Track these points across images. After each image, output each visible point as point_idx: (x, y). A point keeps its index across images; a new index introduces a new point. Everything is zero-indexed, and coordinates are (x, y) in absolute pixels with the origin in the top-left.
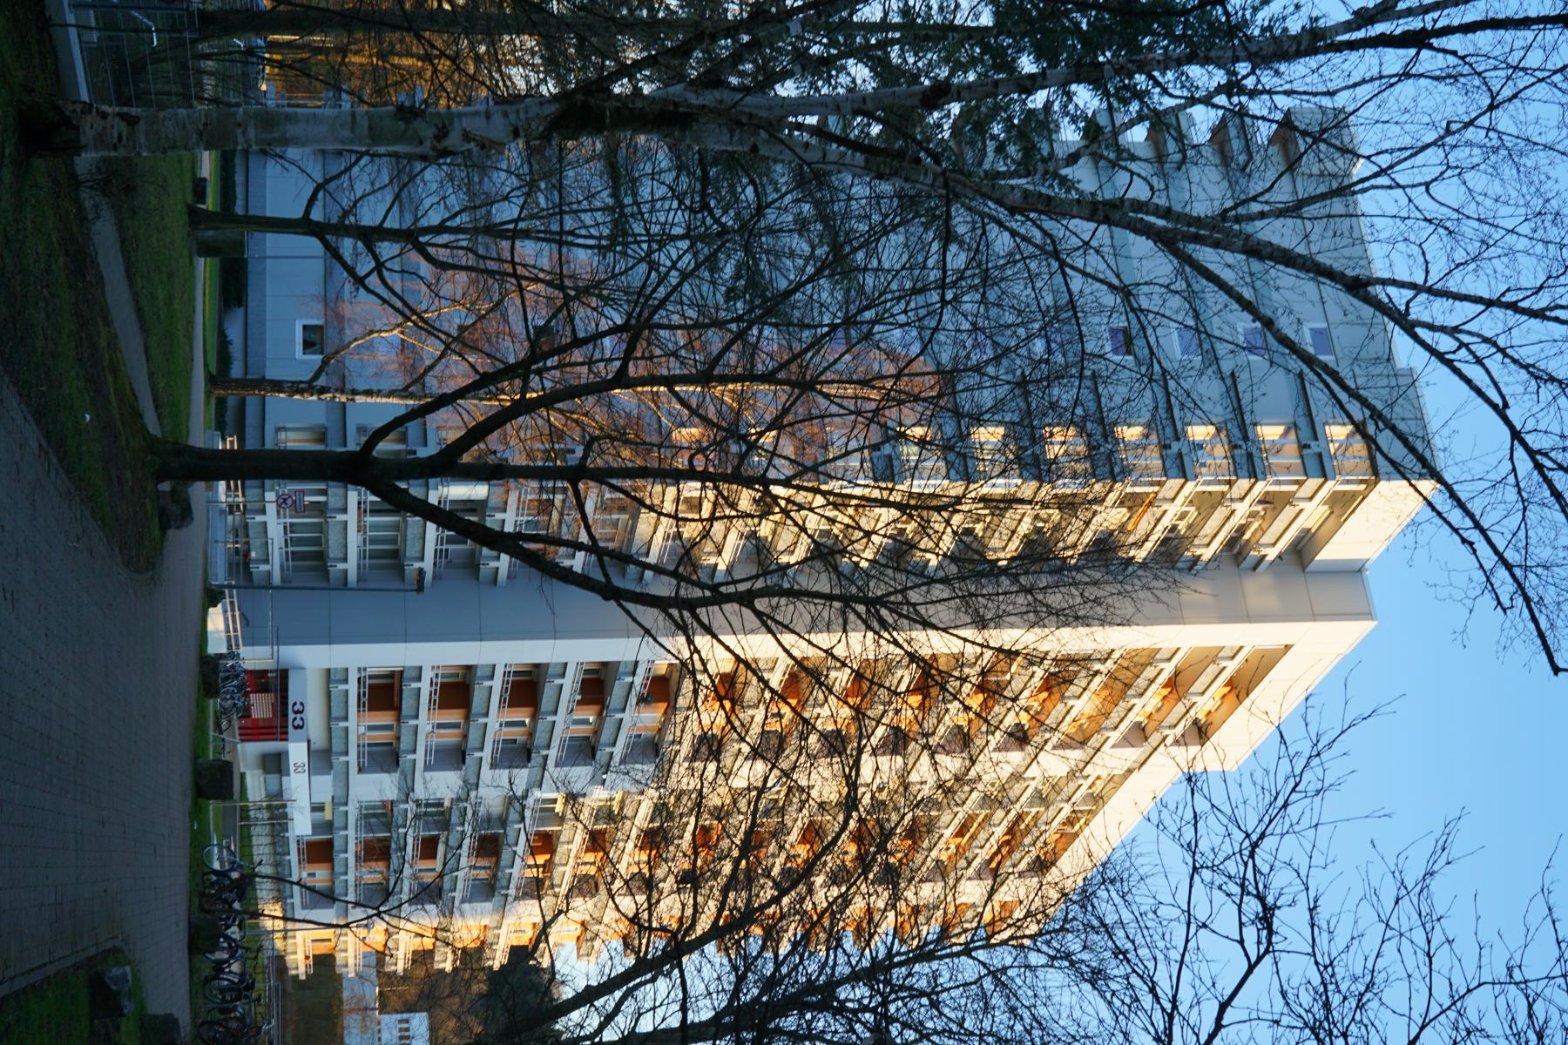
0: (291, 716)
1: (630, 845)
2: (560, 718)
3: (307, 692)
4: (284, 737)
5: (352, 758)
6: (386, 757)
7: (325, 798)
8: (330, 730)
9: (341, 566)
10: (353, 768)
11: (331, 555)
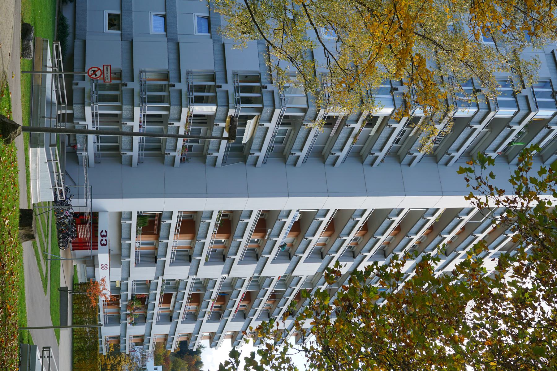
0: (100, 238)
1: (185, 301)
2: (208, 241)
3: (105, 224)
4: (95, 247)
5: (132, 259)
6: (151, 258)
7: (118, 279)
8: (120, 245)
9: (129, 154)
10: (168, 263)
11: (123, 147)
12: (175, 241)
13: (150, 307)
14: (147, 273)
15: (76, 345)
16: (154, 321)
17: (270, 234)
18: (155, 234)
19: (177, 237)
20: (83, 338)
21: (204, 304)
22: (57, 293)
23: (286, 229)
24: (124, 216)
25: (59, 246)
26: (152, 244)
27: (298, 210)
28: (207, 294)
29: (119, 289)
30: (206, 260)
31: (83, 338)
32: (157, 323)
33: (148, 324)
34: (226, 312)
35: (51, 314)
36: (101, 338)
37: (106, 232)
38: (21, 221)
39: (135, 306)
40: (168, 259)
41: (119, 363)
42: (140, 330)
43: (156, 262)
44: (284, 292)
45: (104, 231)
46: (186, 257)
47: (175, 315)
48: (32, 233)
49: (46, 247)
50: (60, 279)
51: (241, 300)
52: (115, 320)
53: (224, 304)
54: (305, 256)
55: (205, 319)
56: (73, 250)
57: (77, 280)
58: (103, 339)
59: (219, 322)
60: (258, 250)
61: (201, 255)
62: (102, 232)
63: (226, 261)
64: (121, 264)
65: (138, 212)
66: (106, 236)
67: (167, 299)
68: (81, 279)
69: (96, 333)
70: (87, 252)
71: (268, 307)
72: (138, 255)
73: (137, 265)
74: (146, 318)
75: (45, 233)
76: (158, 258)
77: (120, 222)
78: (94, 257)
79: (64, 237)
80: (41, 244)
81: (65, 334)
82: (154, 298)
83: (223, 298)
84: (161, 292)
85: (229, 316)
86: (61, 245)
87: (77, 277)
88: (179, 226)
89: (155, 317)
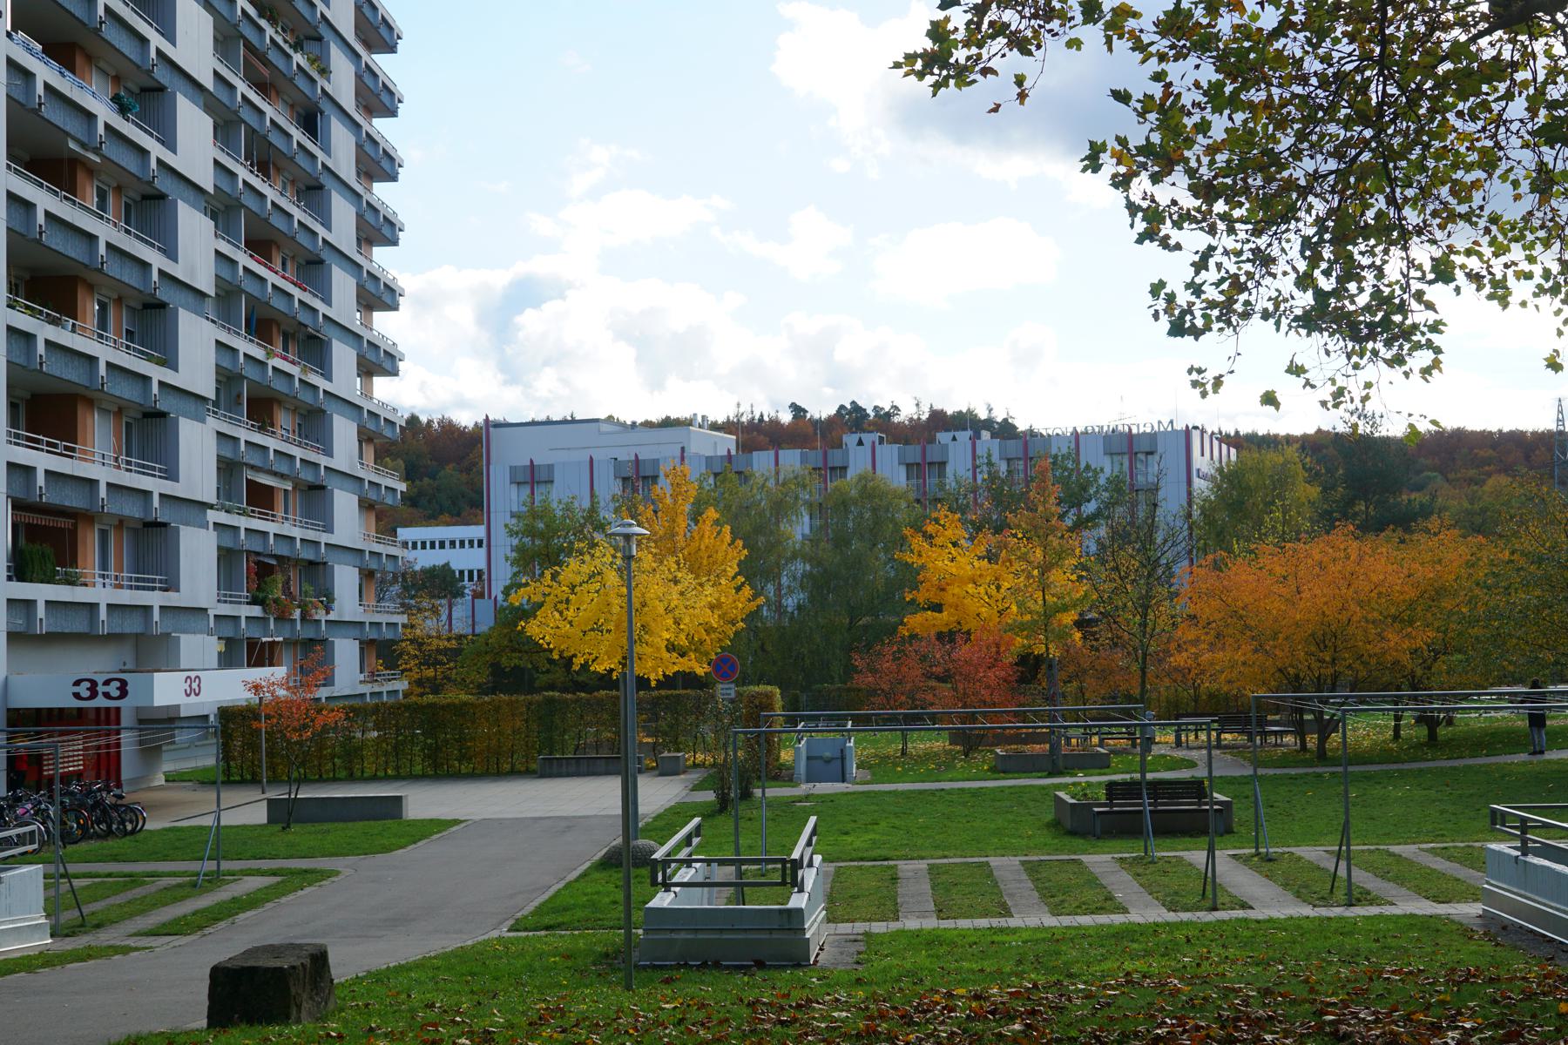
0: (101, 702)
1: (272, 443)
5: (155, 599)
6: (149, 542)
8: (113, 638)
12: (98, 462)
13: (283, 550)
14: (197, 552)
15: (418, 769)
16: (324, 538)
17: (83, 145)
18: (75, 526)
19: (85, 452)
20: (397, 749)
21: (279, 385)
22: (299, 834)
23: (65, 84)
24: (20, 623)
25: (133, 832)
26: (104, 535)
27: (9, 35)
28: (251, 372)
29: (229, 642)
30: (162, 363)
31: (395, 748)
32: (329, 529)
33: (331, 558)
34: (303, 317)
35: (387, 849)
36: (363, 695)
37: (77, 683)
38: (270, 1019)
39: (277, 593)
40: (154, 485)
41: (418, 643)
42: (345, 579)
43: (164, 525)
44: (251, 132)
45: (76, 689)
46: (148, 431)
47: (307, 476)
48: (307, 961)
49: (179, 880)
50: (244, 827)
51: (270, 269)
52: (312, 654)
53: (278, 325)
54: (156, 40)
55: (322, 384)
56: (119, 785)
57: (205, 769)
58: (366, 689)
59: (329, 343)
60: (132, 194)
61: (146, 379)
62: (77, 696)
63: (164, 298)
64: (168, 634)
65: (9, 578)
66: (94, 683)
67: (261, 498)
68: (208, 759)
69: (356, 709)
70: (128, 741)
71: (289, 188)
72: (137, 580)
73: (171, 585)
74: (311, 563)
75: (125, 887)
76: (149, 519)
77: (41, 635)
78: (141, 721)
79: (105, 817)
80: (175, 900)
81: (424, 801)
82: (258, 536)
83: (262, 325)
84: (244, 513)
85: (315, 311)
86: (129, 827)
87: (195, 771)
88: (55, 446)
89: (311, 535)
